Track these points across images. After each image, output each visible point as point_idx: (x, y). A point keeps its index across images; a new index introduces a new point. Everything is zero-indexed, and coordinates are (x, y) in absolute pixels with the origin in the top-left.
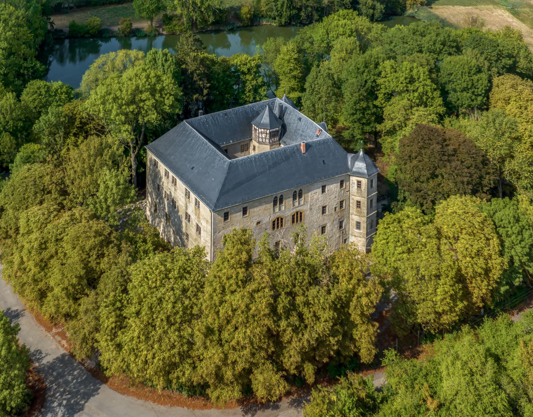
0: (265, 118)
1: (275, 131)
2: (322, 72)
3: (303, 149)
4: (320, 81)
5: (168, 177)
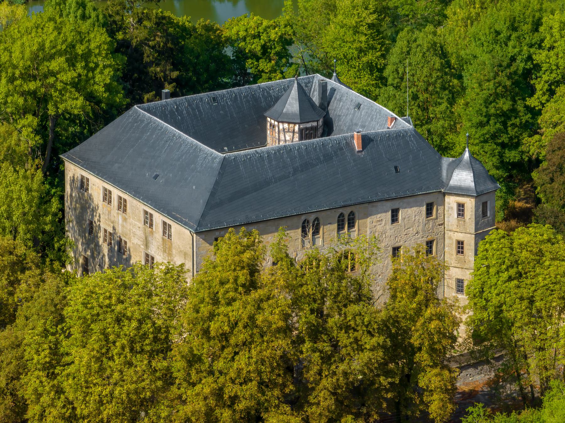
0: (292, 104)
1: (312, 128)
2: (419, 42)
3: (357, 144)
4: (416, 57)
5: (110, 202)
